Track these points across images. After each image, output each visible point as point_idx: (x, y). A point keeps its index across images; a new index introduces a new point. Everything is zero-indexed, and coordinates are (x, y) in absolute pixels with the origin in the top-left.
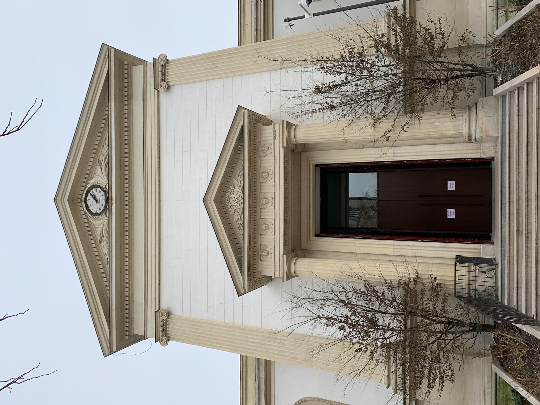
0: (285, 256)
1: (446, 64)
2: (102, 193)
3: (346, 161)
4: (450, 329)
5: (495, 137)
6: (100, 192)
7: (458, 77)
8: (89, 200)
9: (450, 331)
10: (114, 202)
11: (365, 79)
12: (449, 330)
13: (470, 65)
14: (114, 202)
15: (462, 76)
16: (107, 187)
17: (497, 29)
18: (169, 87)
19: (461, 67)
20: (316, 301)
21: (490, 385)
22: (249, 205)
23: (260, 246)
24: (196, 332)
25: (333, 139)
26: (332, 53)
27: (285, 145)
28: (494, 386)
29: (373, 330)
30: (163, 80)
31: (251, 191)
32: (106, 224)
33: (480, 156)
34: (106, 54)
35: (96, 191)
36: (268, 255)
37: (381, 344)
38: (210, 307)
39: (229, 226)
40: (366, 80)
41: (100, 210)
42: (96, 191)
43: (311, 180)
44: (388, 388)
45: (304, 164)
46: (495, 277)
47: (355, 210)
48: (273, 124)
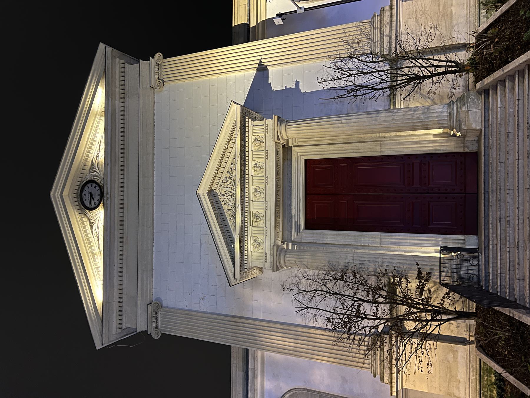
1: (432, 61)
2: (98, 188)
3: (233, 395)
4: (436, 317)
5: (478, 130)
6: (95, 187)
7: (439, 74)
8: (85, 195)
9: (435, 319)
11: (353, 76)
12: (435, 317)
13: (454, 62)
15: (446, 73)
17: (479, 26)
19: (445, 64)
20: (305, 292)
21: (475, 373)
22: (242, 197)
23: (251, 238)
24: (188, 325)
25: (419, 238)
26: (367, 340)
28: (478, 373)
29: (361, 319)
31: (243, 184)
33: (464, 150)
35: (92, 186)
36: (259, 246)
37: (368, 332)
38: (203, 299)
39: (221, 218)
40: (355, 76)
41: (95, 204)
42: (92, 186)
43: (301, 174)
44: (375, 377)
46: (478, 265)
47: (361, 365)
48: (265, 119)
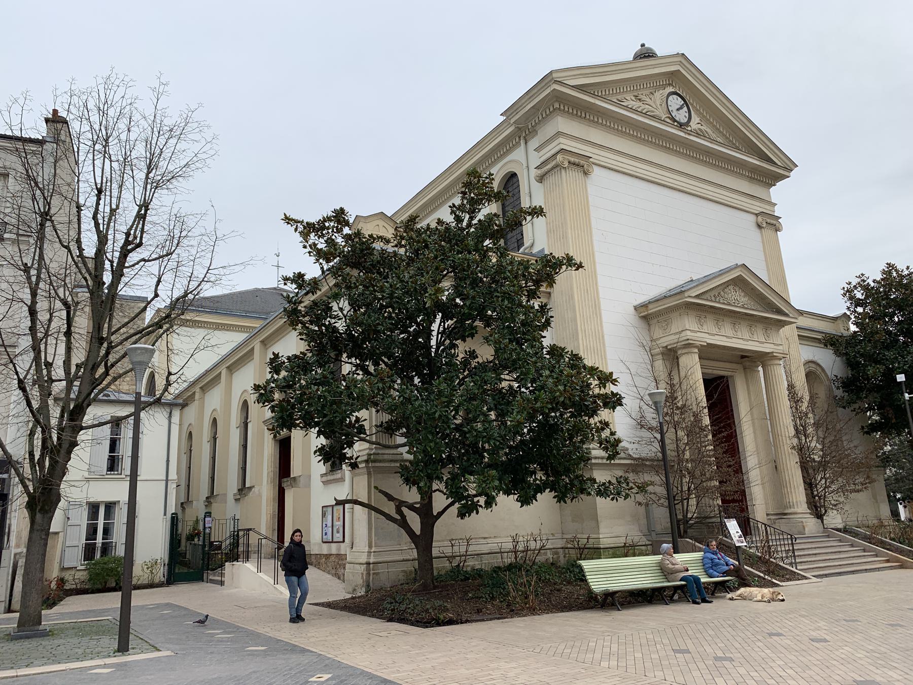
0: (705, 344)
10: (687, 136)
14: (687, 136)
16: (689, 128)
18: (759, 226)
27: (775, 354)
30: (569, 162)
32: (657, 113)
34: (789, 167)
45: (734, 366)
